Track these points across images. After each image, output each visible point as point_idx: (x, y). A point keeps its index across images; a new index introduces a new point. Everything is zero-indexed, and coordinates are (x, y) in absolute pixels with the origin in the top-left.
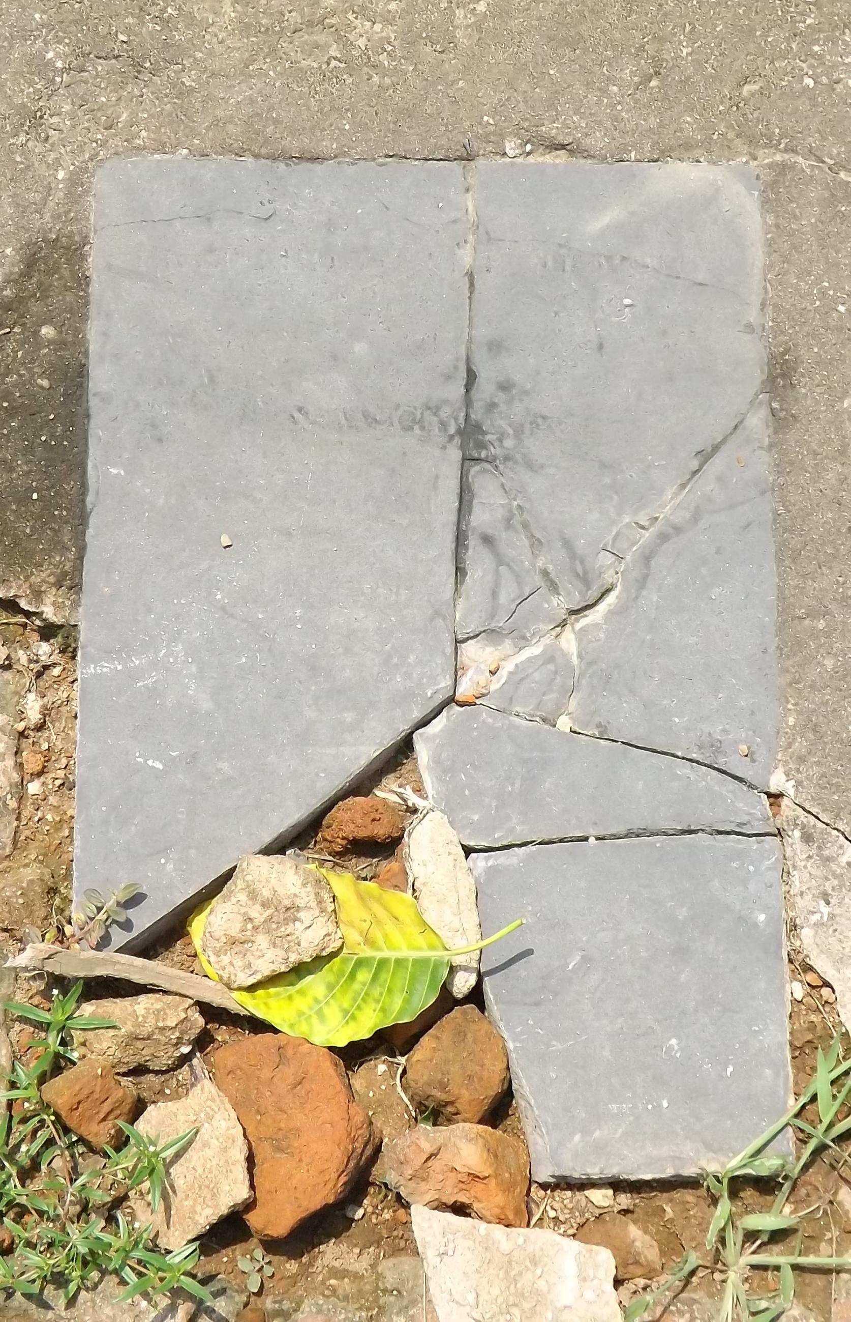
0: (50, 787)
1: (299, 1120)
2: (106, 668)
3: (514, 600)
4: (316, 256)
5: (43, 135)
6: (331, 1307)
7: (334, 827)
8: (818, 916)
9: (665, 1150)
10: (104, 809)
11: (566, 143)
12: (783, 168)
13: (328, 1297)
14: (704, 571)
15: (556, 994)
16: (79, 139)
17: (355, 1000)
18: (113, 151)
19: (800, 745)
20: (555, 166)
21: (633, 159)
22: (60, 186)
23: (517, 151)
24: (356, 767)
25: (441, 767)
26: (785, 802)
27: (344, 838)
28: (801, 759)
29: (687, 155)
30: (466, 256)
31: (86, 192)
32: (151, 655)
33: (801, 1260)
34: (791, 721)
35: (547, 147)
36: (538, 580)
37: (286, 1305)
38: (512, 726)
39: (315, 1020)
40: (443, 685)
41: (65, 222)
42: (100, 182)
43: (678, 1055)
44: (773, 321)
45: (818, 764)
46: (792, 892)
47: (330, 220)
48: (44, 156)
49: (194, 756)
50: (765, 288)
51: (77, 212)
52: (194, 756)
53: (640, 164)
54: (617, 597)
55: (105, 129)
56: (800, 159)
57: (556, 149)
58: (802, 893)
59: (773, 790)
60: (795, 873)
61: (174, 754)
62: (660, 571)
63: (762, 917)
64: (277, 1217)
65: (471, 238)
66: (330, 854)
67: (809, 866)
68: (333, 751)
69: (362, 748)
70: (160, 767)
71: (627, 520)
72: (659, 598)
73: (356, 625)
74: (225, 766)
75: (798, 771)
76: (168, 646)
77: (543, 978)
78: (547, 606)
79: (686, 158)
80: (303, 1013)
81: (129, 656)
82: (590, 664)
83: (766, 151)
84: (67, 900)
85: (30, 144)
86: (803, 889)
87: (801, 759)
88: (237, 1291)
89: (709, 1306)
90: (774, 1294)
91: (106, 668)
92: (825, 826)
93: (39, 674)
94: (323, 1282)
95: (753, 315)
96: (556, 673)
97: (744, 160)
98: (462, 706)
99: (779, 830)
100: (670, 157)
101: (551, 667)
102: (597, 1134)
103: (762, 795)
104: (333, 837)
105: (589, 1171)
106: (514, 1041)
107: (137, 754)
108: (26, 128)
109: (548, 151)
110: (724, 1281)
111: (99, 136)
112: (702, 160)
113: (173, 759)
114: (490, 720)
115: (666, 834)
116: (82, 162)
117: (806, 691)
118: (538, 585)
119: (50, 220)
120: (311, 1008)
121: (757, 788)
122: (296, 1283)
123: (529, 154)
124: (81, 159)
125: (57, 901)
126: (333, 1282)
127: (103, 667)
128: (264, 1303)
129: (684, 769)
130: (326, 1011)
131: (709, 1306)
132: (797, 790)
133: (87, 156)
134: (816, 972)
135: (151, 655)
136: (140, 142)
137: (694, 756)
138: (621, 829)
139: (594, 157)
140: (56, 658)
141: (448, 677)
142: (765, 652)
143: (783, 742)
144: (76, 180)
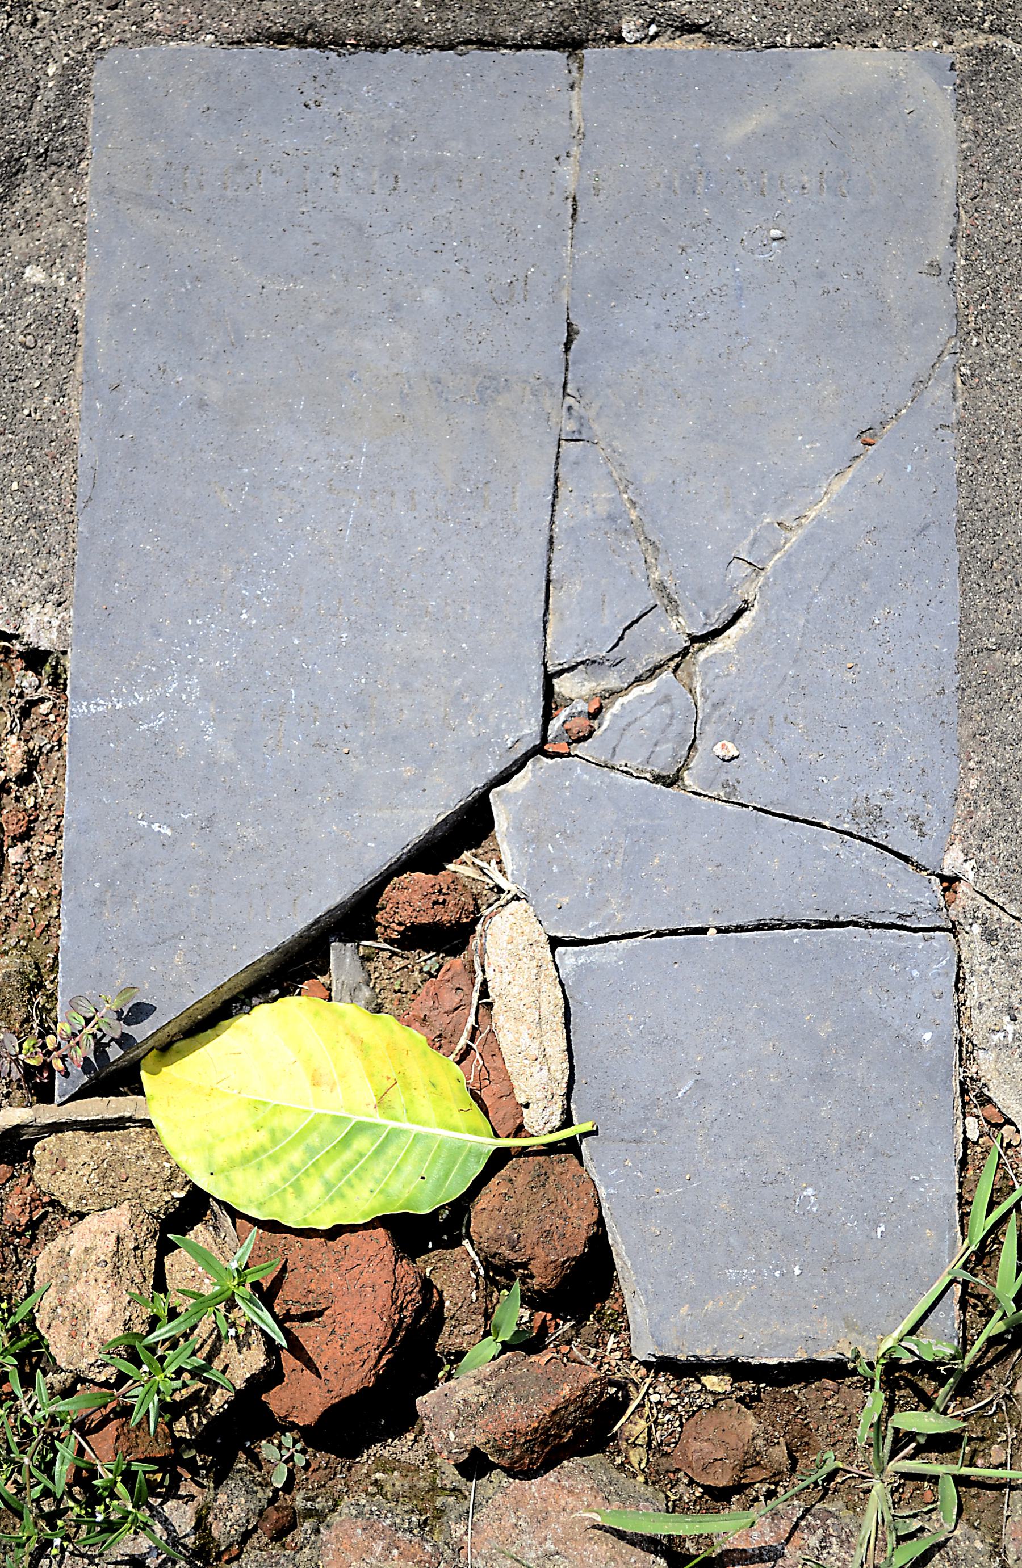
0: (37, 853)
1: (333, 1281)
2: (100, 706)
3: (621, 622)
4: (376, 175)
5: (29, 17)
6: (374, 1508)
7: (387, 909)
8: (1001, 1035)
9: (796, 1328)
10: (97, 885)
11: (701, 22)
12: (988, 54)
13: (373, 1495)
14: (865, 587)
15: (662, 1129)
16: (76, 21)
17: (344, 1172)
18: (118, 38)
19: (983, 815)
20: (687, 54)
21: (788, 43)
22: (50, 84)
23: (638, 35)
24: (415, 835)
25: (531, 839)
26: (962, 887)
27: (400, 924)
28: (985, 834)
29: (861, 37)
30: (568, 174)
31: (84, 92)
32: (159, 690)
33: (966, 1471)
34: (973, 783)
35: (677, 28)
36: (651, 597)
37: (320, 1504)
38: (613, 784)
39: (290, 1198)
40: (527, 731)
41: (57, 131)
42: (100, 79)
43: (815, 1209)
44: (966, 259)
45: (1007, 840)
46: (968, 1004)
47: (393, 126)
48: (30, 45)
49: (211, 820)
50: (957, 215)
51: (71, 118)
52: (211, 820)
53: (797, 50)
54: (754, 620)
55: (108, 8)
56: (1009, 43)
57: (690, 32)
58: (980, 1006)
59: (946, 872)
60: (973, 979)
61: (186, 817)
62: (810, 587)
63: (928, 1036)
64: (301, 1399)
65: (575, 150)
66: (385, 941)
67: (990, 971)
68: (387, 814)
69: (422, 812)
70: (169, 832)
71: (768, 520)
72: (807, 621)
73: (416, 654)
74: (249, 832)
75: (980, 848)
76: (181, 680)
77: (645, 1107)
78: (663, 630)
79: (858, 42)
80: (276, 1188)
81: (131, 693)
82: (715, 706)
83: (965, 31)
84: (52, 997)
85: (13, 29)
86: (983, 1000)
87: (985, 834)
88: (260, 1484)
89: (848, 1521)
90: (930, 1507)
91: (100, 706)
92: (1013, 921)
93: (25, 713)
94: (368, 1475)
95: (940, 251)
96: (672, 717)
97: (935, 44)
98: (552, 758)
99: (953, 923)
100: (838, 40)
101: (665, 709)
102: (710, 1306)
103: (933, 877)
104: (388, 922)
105: (698, 1353)
106: (607, 1187)
107: (140, 817)
108: (8, 8)
109: (678, 33)
110: (868, 1491)
111: (101, 18)
112: (879, 44)
113: (184, 823)
114: (586, 777)
115: (807, 926)
116: (79, 53)
117: (994, 744)
118: (652, 603)
119: (37, 129)
120: (285, 1180)
121: (926, 870)
122: (335, 1474)
123: (653, 38)
124: (78, 49)
125: (41, 999)
126: (379, 1476)
127: (98, 705)
128: (293, 1500)
129: (829, 842)
130: (305, 1183)
131: (848, 1521)
132: (977, 873)
133: (86, 44)
134: (996, 1106)
135: (159, 690)
136: (150, 25)
137: (846, 827)
138: (750, 920)
139: (737, 41)
140: (44, 691)
141: (533, 721)
142: (942, 692)
143: (961, 810)
144: (70, 77)
